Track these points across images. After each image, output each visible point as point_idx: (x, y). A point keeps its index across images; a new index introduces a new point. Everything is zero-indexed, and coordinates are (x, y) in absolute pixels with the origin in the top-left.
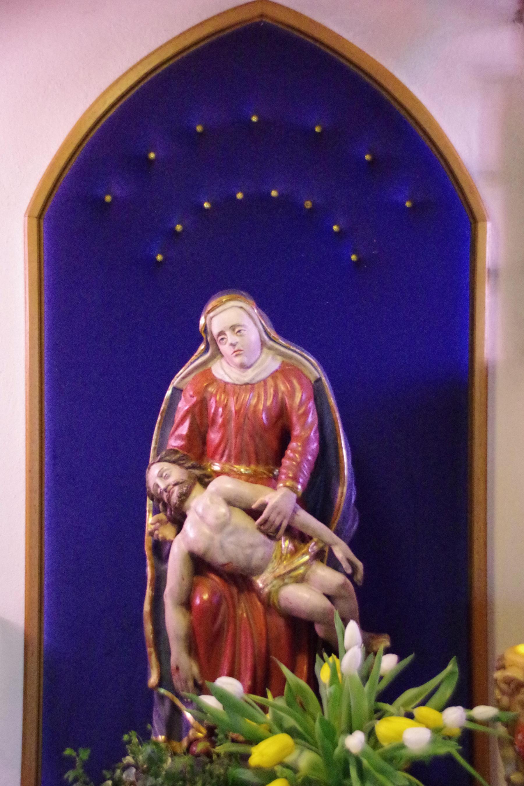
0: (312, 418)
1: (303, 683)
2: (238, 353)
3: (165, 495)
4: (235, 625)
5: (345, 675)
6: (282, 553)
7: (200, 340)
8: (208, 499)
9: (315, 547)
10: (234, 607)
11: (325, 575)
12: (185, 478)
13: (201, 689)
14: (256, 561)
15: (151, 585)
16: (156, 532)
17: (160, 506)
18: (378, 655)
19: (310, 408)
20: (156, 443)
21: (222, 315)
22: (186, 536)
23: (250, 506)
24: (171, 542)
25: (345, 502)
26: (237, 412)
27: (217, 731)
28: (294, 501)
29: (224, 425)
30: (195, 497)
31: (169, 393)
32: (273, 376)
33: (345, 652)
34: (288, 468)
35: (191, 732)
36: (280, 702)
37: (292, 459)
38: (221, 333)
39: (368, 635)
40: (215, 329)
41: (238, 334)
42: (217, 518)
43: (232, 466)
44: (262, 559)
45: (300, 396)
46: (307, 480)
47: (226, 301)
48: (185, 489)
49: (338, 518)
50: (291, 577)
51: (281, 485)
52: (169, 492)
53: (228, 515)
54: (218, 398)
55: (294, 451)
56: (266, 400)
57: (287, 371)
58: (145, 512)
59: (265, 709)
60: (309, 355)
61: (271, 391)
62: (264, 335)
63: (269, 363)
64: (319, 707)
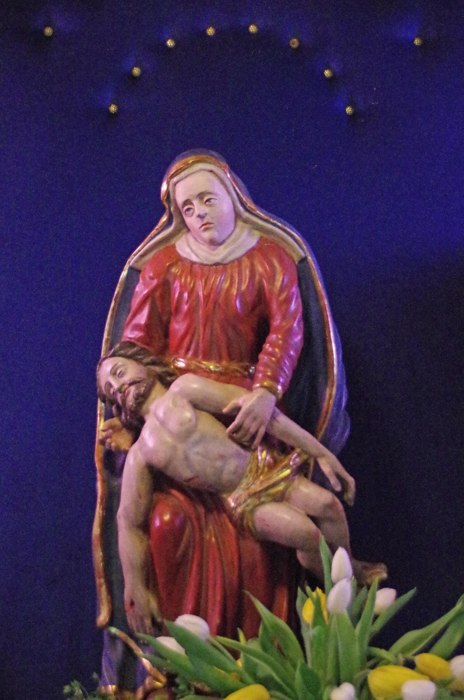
0: (295, 305)
1: (282, 623)
2: (206, 226)
3: (119, 397)
4: (202, 553)
5: (331, 613)
6: (258, 466)
7: (162, 210)
8: (171, 401)
9: (297, 460)
10: (201, 529)
11: (308, 491)
12: (143, 376)
13: (159, 629)
14: (226, 476)
15: (101, 504)
16: (108, 440)
17: (114, 408)
18: (372, 589)
19: (293, 293)
20: (109, 335)
21: (188, 179)
22: (145, 444)
23: (221, 410)
24: (126, 453)
25: (334, 405)
26: (207, 298)
27: (178, 680)
28: (273, 404)
29: (191, 312)
30: (154, 399)
31: (124, 274)
32: (250, 254)
33: (333, 585)
34: (266, 365)
35: (148, 681)
36: (254, 645)
37: (272, 354)
38: (187, 202)
39: (360, 565)
40: (180, 199)
41: (207, 203)
42: (181, 424)
43: (200, 362)
44: (235, 473)
45: (281, 279)
46: (289, 380)
47: (193, 163)
48: (143, 389)
49: (325, 426)
50: (269, 495)
51: (258, 385)
52: (124, 392)
53: (194, 420)
54: (183, 280)
55: (273, 345)
56: (240, 283)
57: (266, 248)
58: (96, 416)
59: (235, 655)
60: (294, 231)
61: (247, 273)
62: (238, 205)
63: (244, 240)
64: (301, 653)
